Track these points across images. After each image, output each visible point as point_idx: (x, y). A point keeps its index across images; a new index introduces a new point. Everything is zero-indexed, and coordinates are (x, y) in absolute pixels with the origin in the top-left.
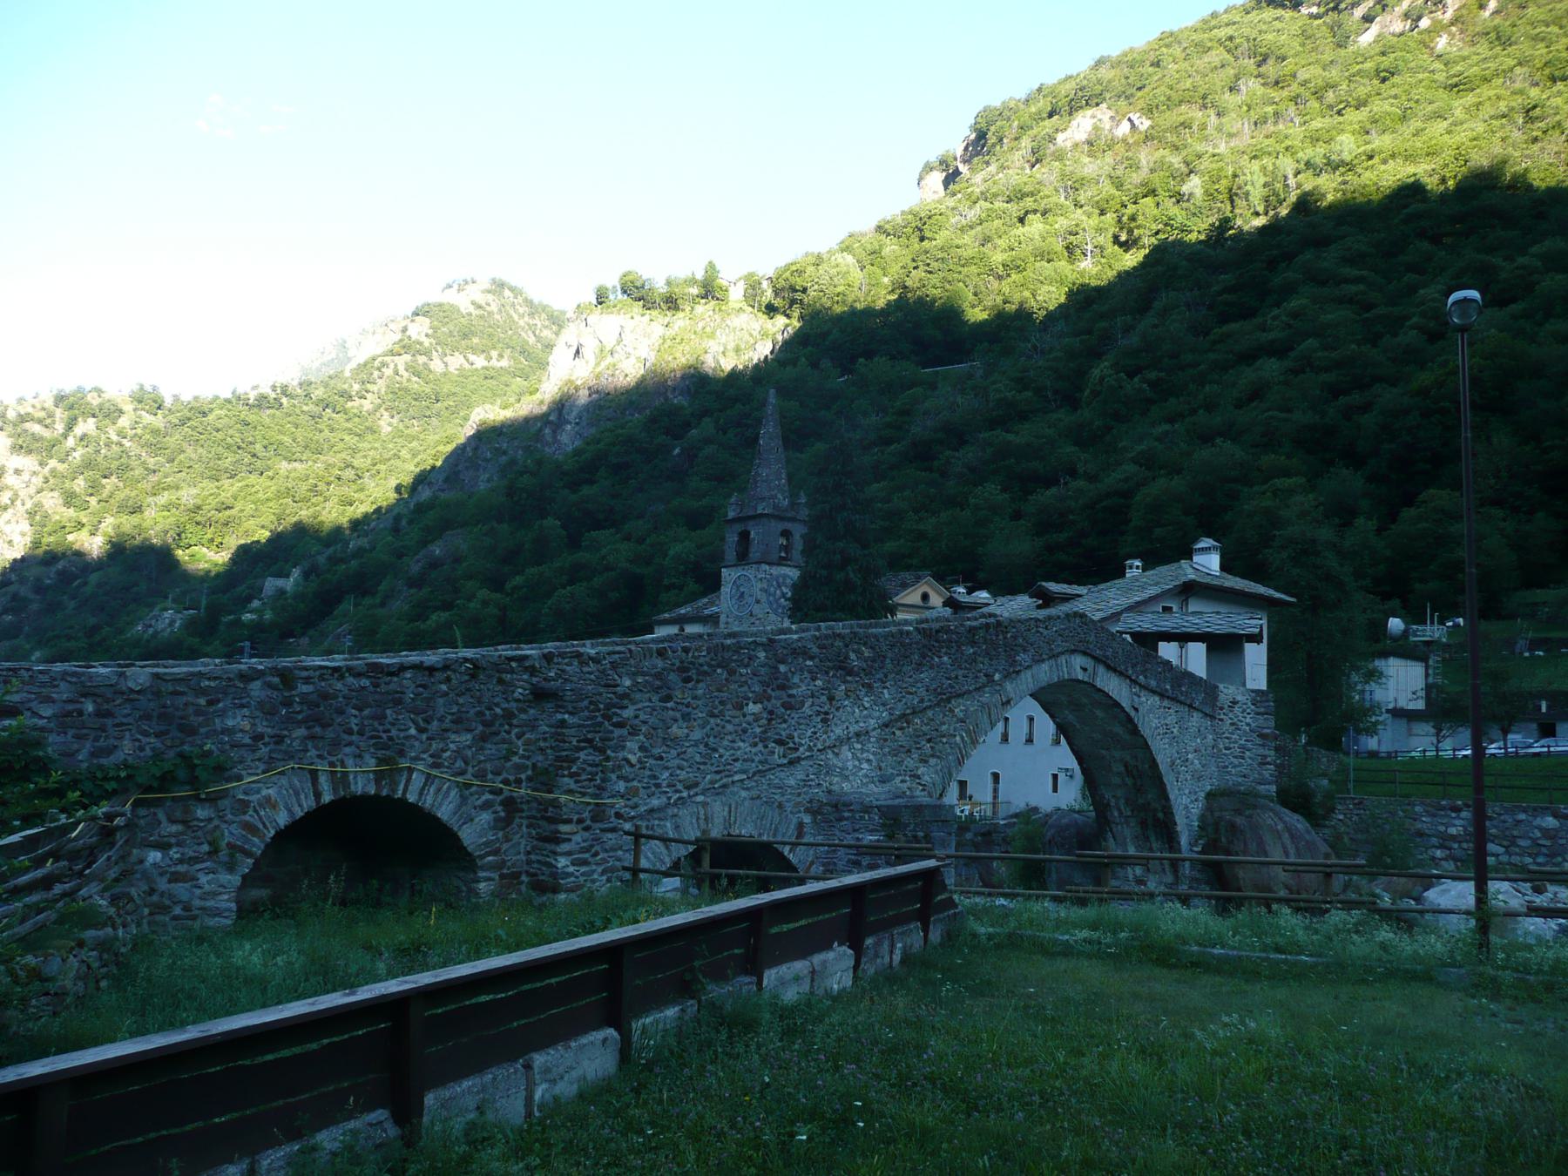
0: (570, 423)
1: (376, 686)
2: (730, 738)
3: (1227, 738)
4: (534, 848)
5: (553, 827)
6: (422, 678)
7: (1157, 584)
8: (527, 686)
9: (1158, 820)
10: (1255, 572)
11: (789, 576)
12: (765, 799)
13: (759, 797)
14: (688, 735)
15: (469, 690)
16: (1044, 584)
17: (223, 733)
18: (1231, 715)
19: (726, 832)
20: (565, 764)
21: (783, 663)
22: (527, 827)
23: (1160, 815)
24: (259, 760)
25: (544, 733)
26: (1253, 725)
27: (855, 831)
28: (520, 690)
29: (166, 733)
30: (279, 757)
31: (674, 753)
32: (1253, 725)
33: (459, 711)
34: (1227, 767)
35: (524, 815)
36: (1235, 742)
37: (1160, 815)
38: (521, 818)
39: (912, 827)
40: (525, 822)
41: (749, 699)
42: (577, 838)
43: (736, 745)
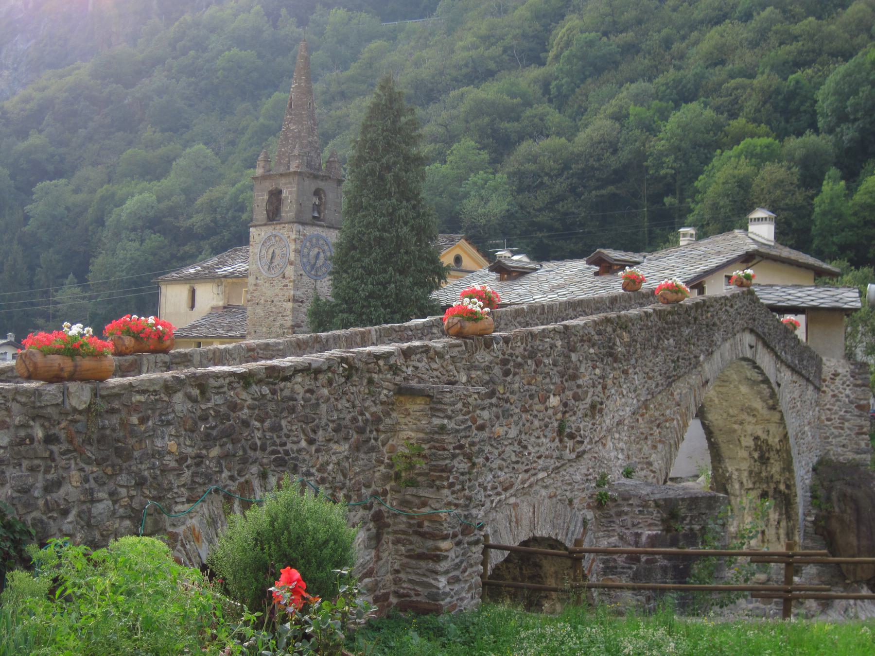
0: (7, 68)
1: (274, 392)
2: (535, 434)
3: (829, 410)
4: (404, 566)
5: (430, 543)
6: (308, 383)
7: (719, 253)
8: (391, 387)
9: (780, 492)
10: (801, 245)
11: (322, 237)
12: (559, 497)
13: (555, 496)
14: (507, 433)
15: (345, 393)
16: (603, 251)
17: (153, 456)
18: (832, 387)
19: (531, 535)
20: (444, 475)
21: (574, 352)
22: (393, 543)
23: (782, 487)
24: (184, 485)
25: (408, 438)
26: (852, 396)
27: (634, 525)
28: (385, 392)
29: (105, 460)
30: (201, 481)
31: (496, 452)
32: (852, 396)
33: (339, 419)
34: (828, 437)
35: (390, 530)
36: (836, 413)
37: (782, 487)
38: (388, 533)
39: (688, 519)
40: (391, 538)
41: (549, 391)
42: (452, 554)
43: (540, 441)
